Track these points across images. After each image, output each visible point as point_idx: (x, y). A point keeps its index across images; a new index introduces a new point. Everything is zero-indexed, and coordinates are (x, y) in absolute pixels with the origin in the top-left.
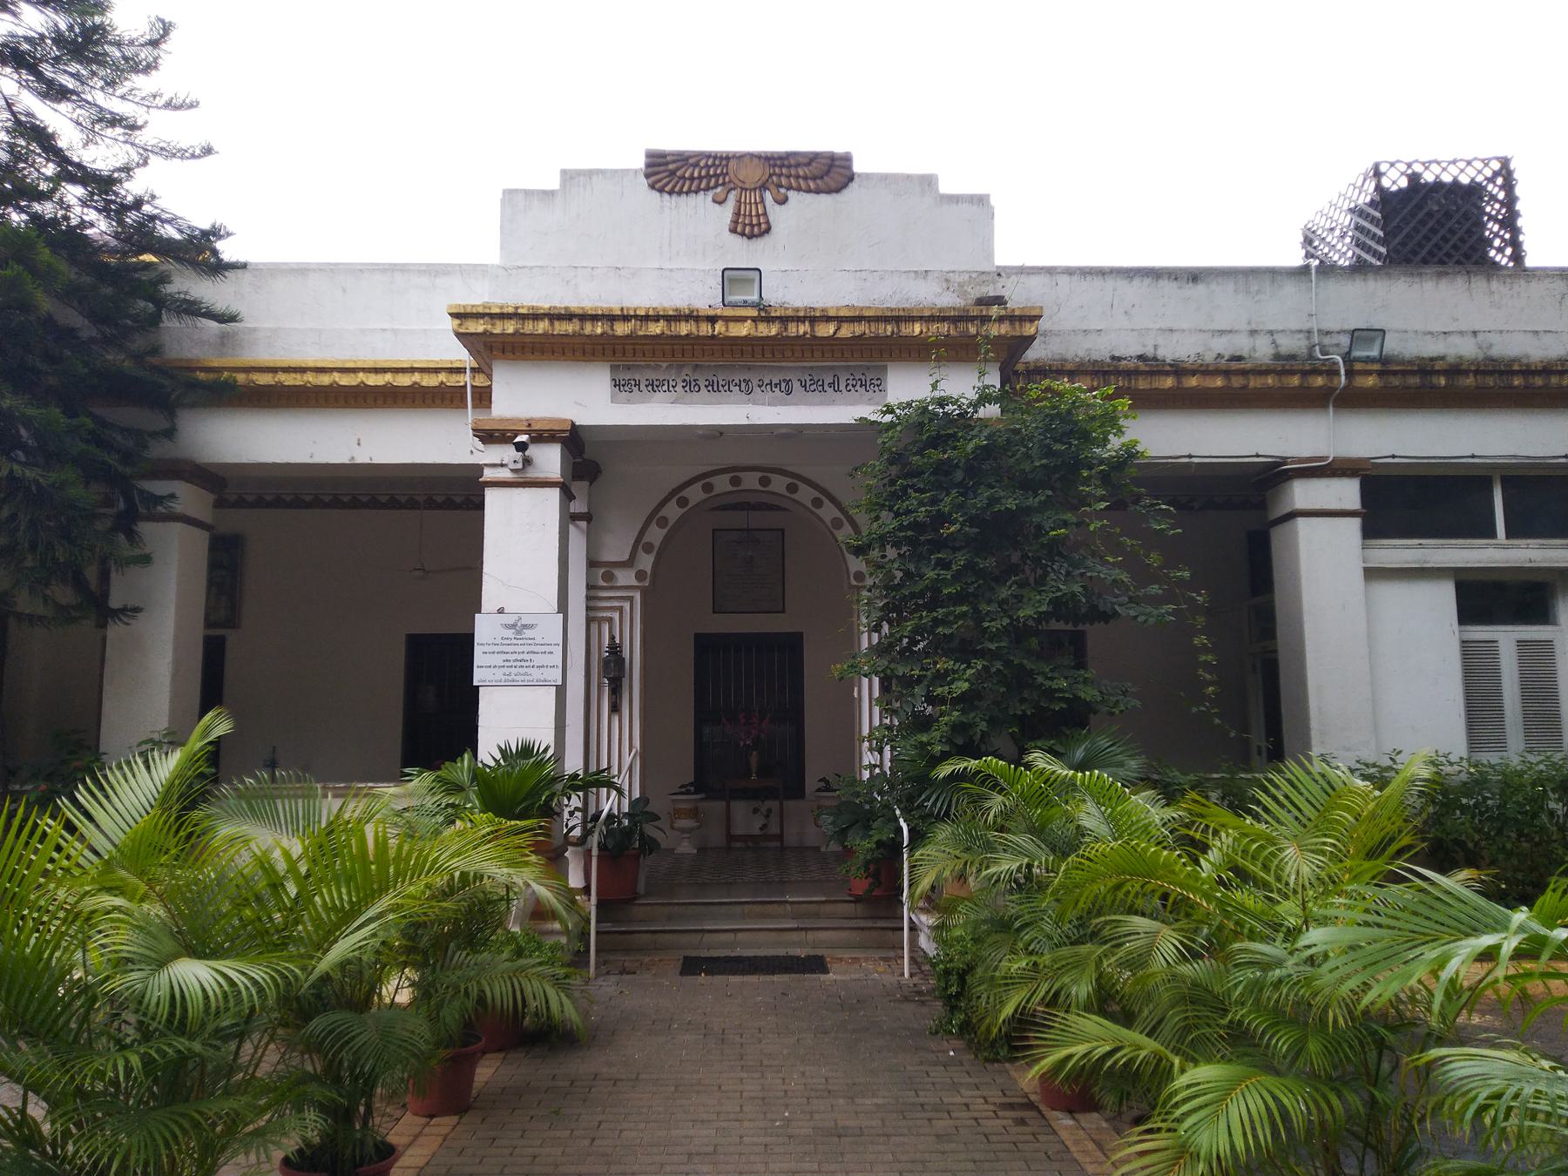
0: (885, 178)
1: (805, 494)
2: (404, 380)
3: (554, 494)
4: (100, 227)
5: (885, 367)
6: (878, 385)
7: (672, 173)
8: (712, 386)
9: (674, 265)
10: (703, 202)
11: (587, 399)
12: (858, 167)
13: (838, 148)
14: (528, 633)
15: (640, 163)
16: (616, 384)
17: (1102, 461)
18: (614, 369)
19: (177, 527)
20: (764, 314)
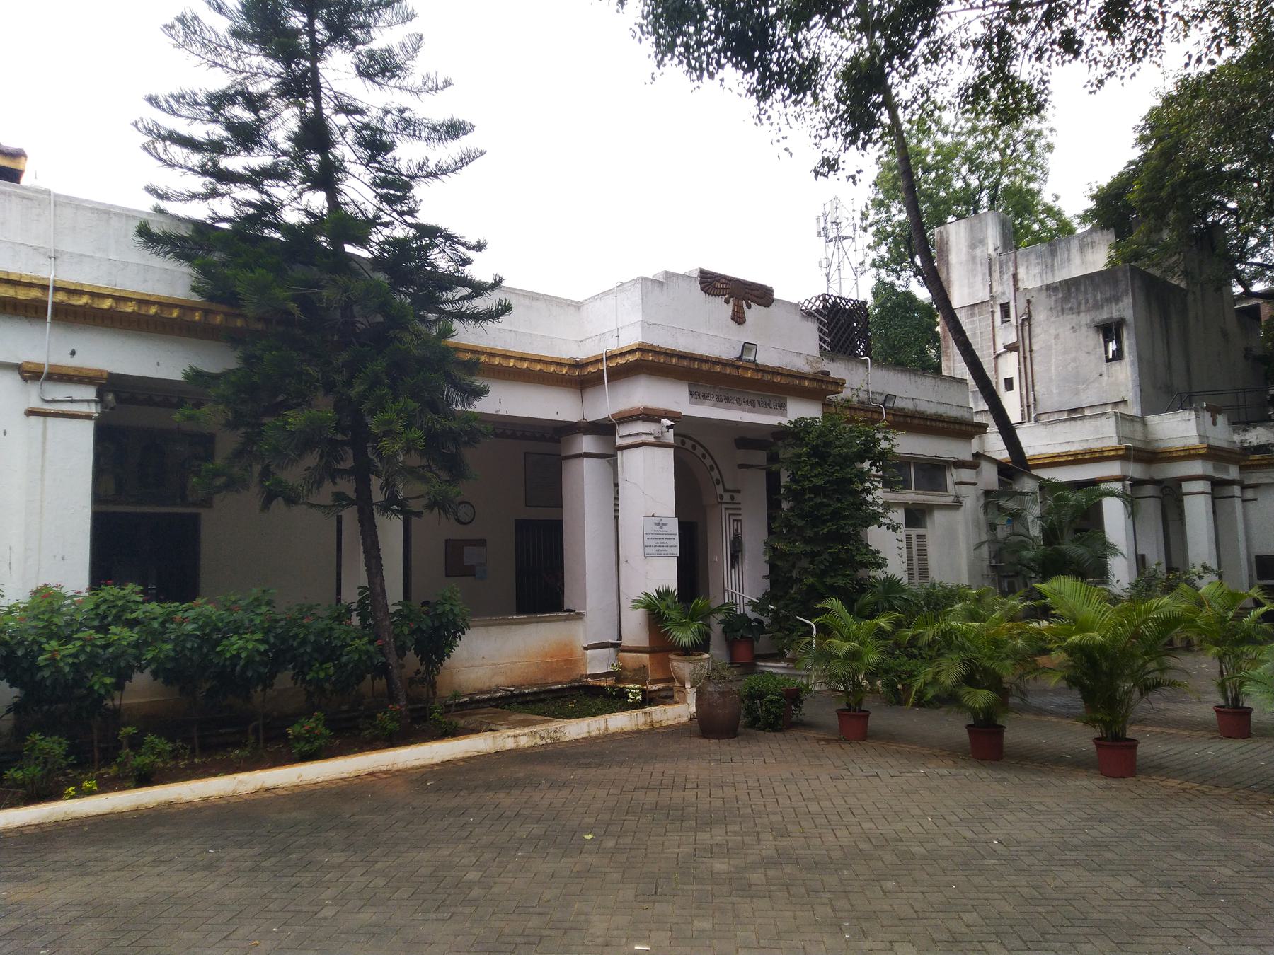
0: (784, 302)
1: (699, 451)
2: (22, 294)
3: (671, 451)
4: (251, 211)
5: (785, 399)
6: (782, 407)
7: (711, 283)
8: (719, 399)
9: (710, 334)
10: (720, 301)
11: (673, 398)
12: (776, 295)
13: (769, 285)
14: (665, 528)
15: (696, 274)
16: (691, 394)
17: (454, 415)
18: (690, 385)
19: (587, 462)
20: (758, 368)
